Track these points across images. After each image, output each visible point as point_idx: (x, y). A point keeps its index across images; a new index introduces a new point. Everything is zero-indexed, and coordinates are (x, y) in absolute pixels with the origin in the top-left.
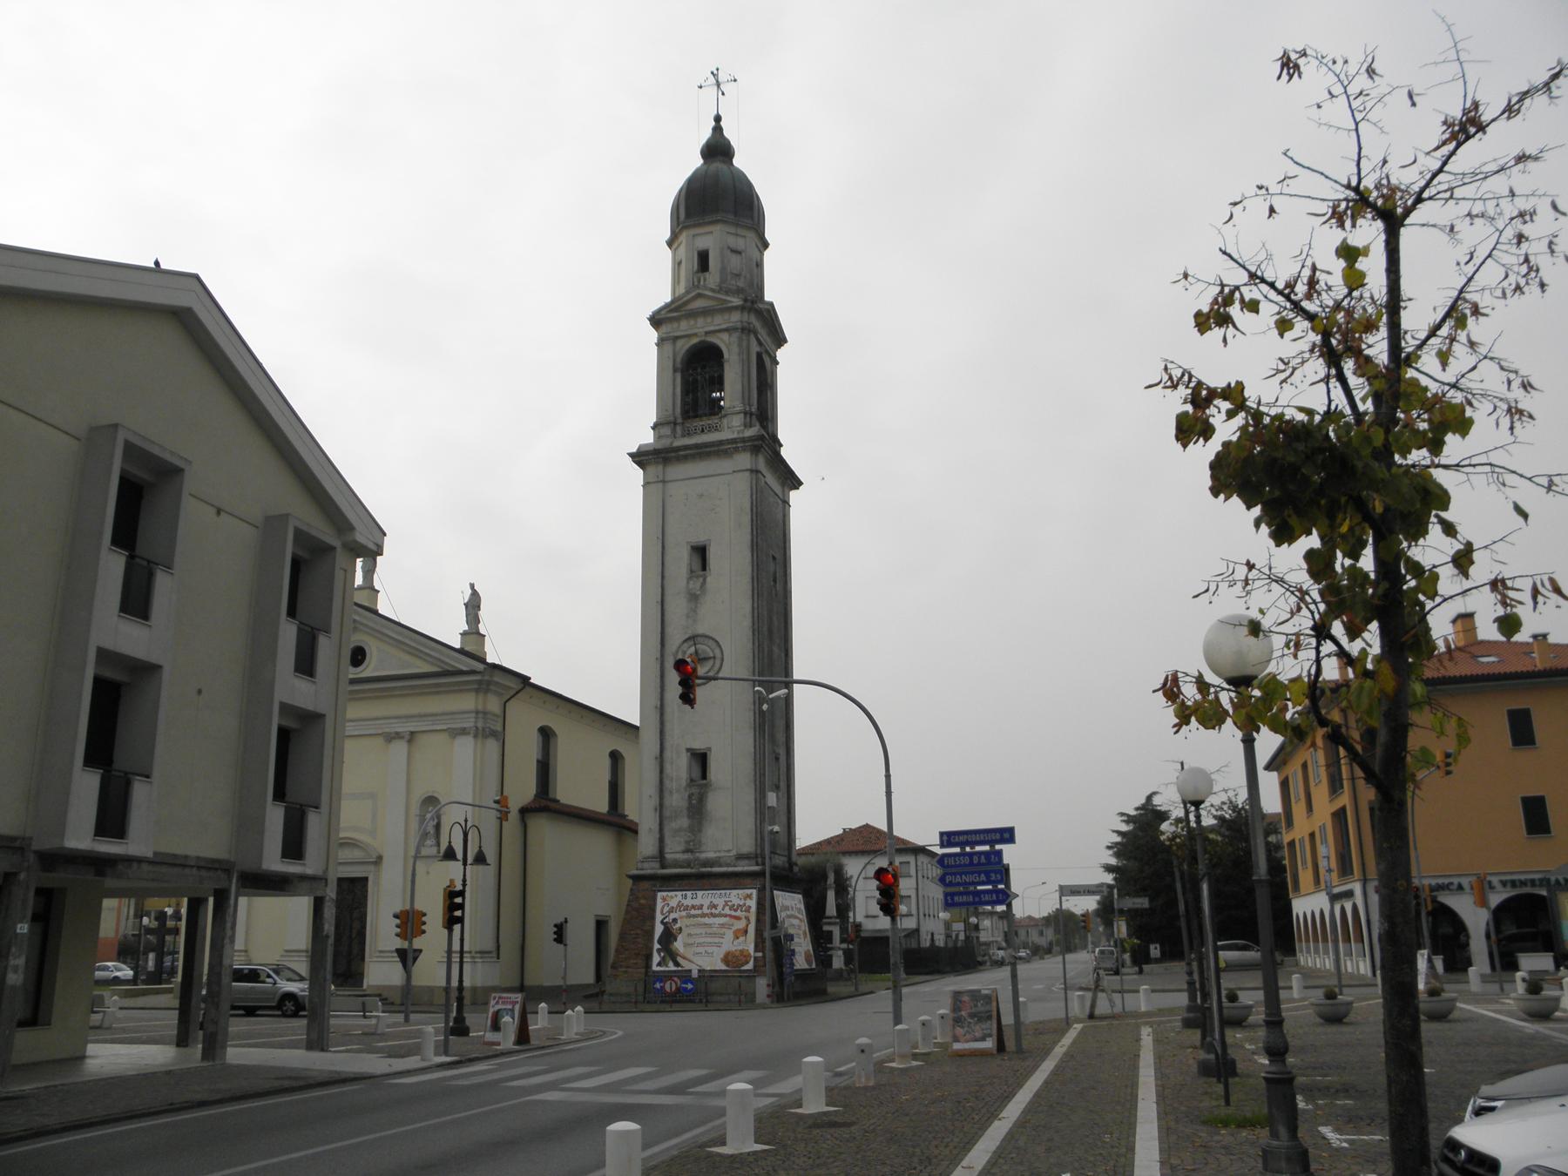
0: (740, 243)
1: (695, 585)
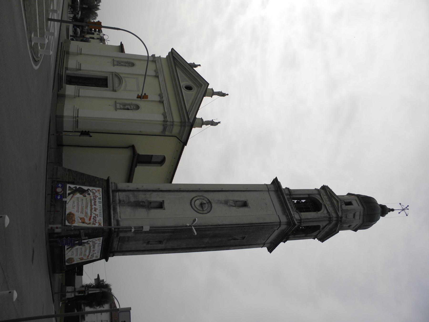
0: (357, 217)
1: (231, 203)
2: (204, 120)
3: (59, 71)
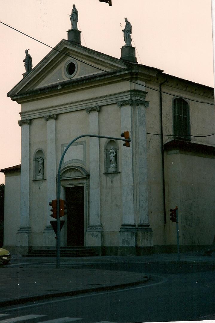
2: (124, 44)
3: (54, 266)
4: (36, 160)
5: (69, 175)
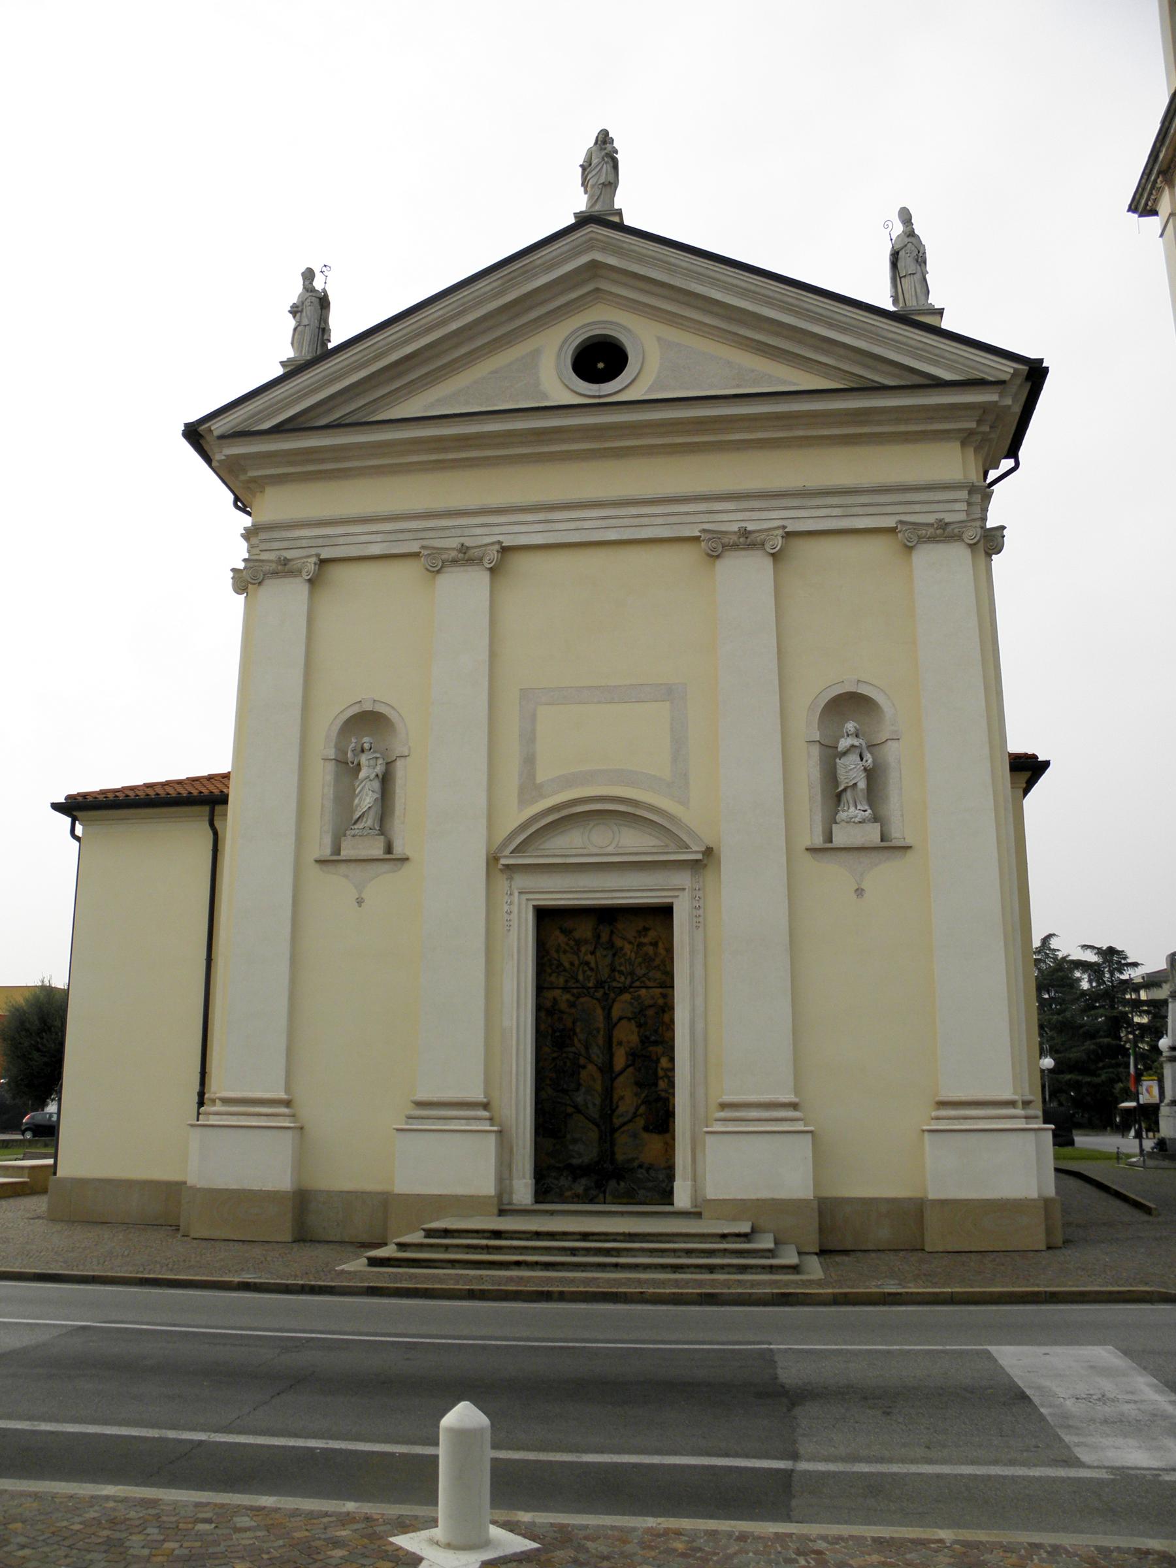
4: (347, 768)
5: (573, 843)
